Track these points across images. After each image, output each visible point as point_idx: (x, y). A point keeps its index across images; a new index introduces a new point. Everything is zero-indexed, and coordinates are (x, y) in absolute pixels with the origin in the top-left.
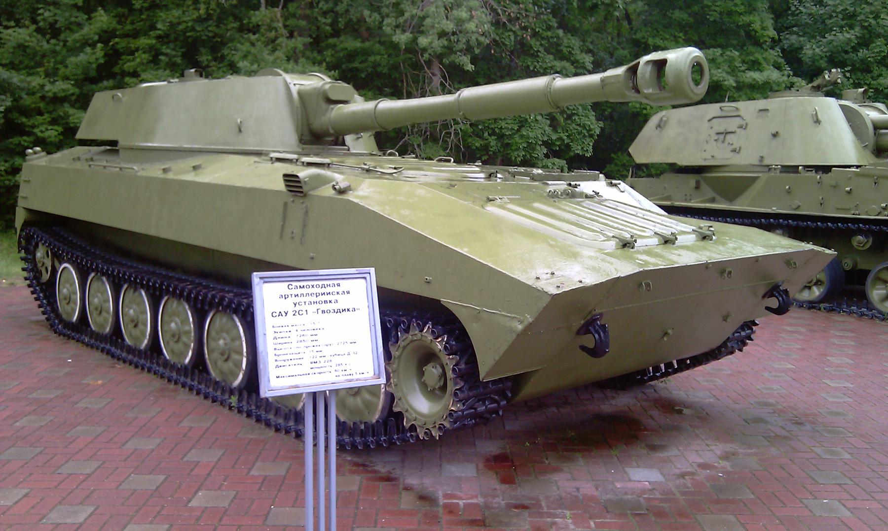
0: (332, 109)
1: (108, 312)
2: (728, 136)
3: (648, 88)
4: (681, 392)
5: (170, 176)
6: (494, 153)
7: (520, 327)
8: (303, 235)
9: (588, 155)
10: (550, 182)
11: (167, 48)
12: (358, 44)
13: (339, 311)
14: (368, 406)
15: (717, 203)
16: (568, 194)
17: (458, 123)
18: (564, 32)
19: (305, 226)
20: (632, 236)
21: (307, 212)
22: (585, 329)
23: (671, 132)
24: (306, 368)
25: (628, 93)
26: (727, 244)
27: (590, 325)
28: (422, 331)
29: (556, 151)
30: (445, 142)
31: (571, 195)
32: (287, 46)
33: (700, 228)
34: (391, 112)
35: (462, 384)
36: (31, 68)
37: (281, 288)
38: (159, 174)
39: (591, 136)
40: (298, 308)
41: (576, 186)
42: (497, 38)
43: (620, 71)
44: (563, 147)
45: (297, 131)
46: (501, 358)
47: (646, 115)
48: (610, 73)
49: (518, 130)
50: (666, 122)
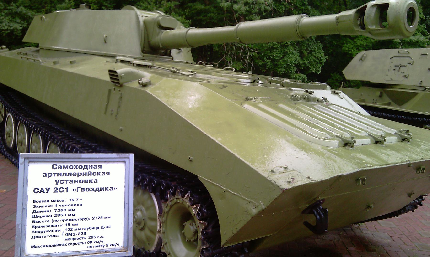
0: (162, 32)
1: (25, 145)
2: (402, 68)
3: (373, 25)
4: (369, 232)
5: (57, 67)
6: (269, 68)
7: (255, 211)
8: (118, 114)
9: (319, 73)
10: (293, 89)
11: (106, 3)
12: (203, 7)
13: (97, 190)
14: (149, 239)
15: (392, 106)
16: (305, 99)
17: (251, 52)
18: (312, 8)
19: (119, 107)
20: (352, 138)
21: (121, 97)
22: (310, 210)
23: (368, 63)
24: (61, 240)
25: (356, 29)
26: (420, 145)
27: (314, 207)
28: (183, 197)
29: (301, 69)
30: (244, 61)
31: (307, 99)
32: (166, 5)
33: (401, 132)
34: (196, 35)
35: (208, 245)
36: (39, 9)
37: (47, 167)
38: (51, 65)
39: (321, 63)
40: (59, 186)
41: (310, 93)
42: (276, 8)
43: (352, 12)
44: (305, 68)
45: (141, 45)
46: (238, 232)
47: (351, 54)
48: (343, 13)
49: (283, 58)
50: (365, 57)
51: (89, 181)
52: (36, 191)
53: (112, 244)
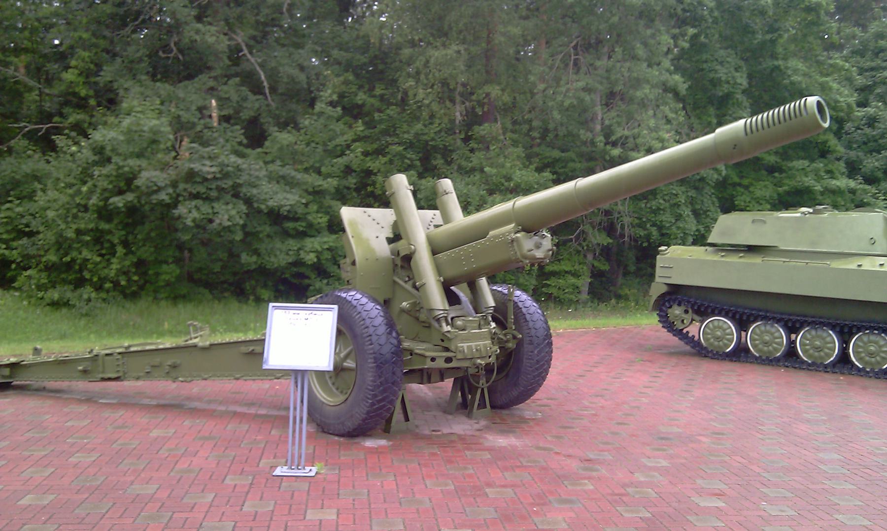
5: (862, 268)
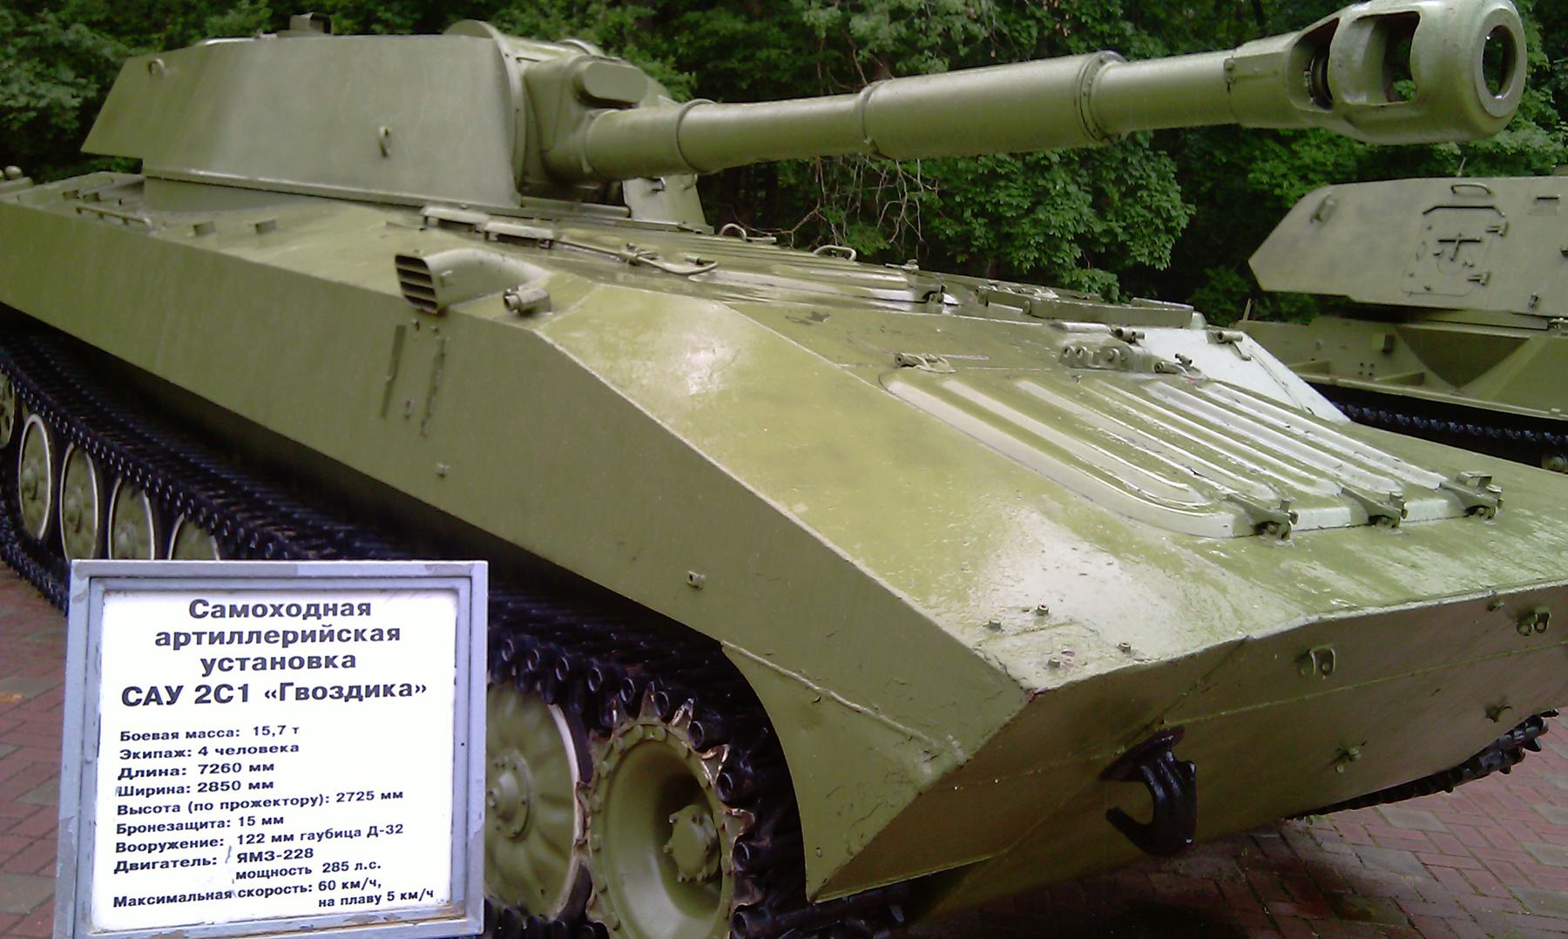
0: (592, 118)
1: (90, 530)
2: (1464, 248)
3: (1358, 90)
4: (1346, 849)
5: (209, 243)
6: (981, 250)
7: (929, 772)
8: (429, 415)
9: (1162, 267)
10: (1068, 324)
11: (386, 10)
12: (739, 25)
13: (355, 693)
14: (544, 875)
15: (1430, 387)
16: (1110, 360)
17: (916, 189)
18: (1136, 28)
19: (434, 390)
20: (1285, 505)
21: (442, 356)
22: (1130, 767)
23: (1342, 230)
24: (222, 876)
25: (1297, 105)
26: (1530, 531)
27: (1146, 757)
28: (667, 719)
29: (1097, 254)
30: (889, 222)
31: (1121, 361)
32: (605, 19)
33: (1462, 481)
34: (714, 128)
35: (758, 897)
36: (142, 31)
37: (172, 612)
38: (186, 238)
39: (1170, 231)
40: (216, 678)
41: (1132, 340)
42: (1005, 31)
43: (1282, 44)
44: (1113, 248)
45: (513, 163)
46: (867, 848)
47: (1280, 198)
48: (1251, 49)
49: (1031, 210)
50: (1333, 209)
51: (323, 662)
52: (133, 696)
53: (407, 891)
